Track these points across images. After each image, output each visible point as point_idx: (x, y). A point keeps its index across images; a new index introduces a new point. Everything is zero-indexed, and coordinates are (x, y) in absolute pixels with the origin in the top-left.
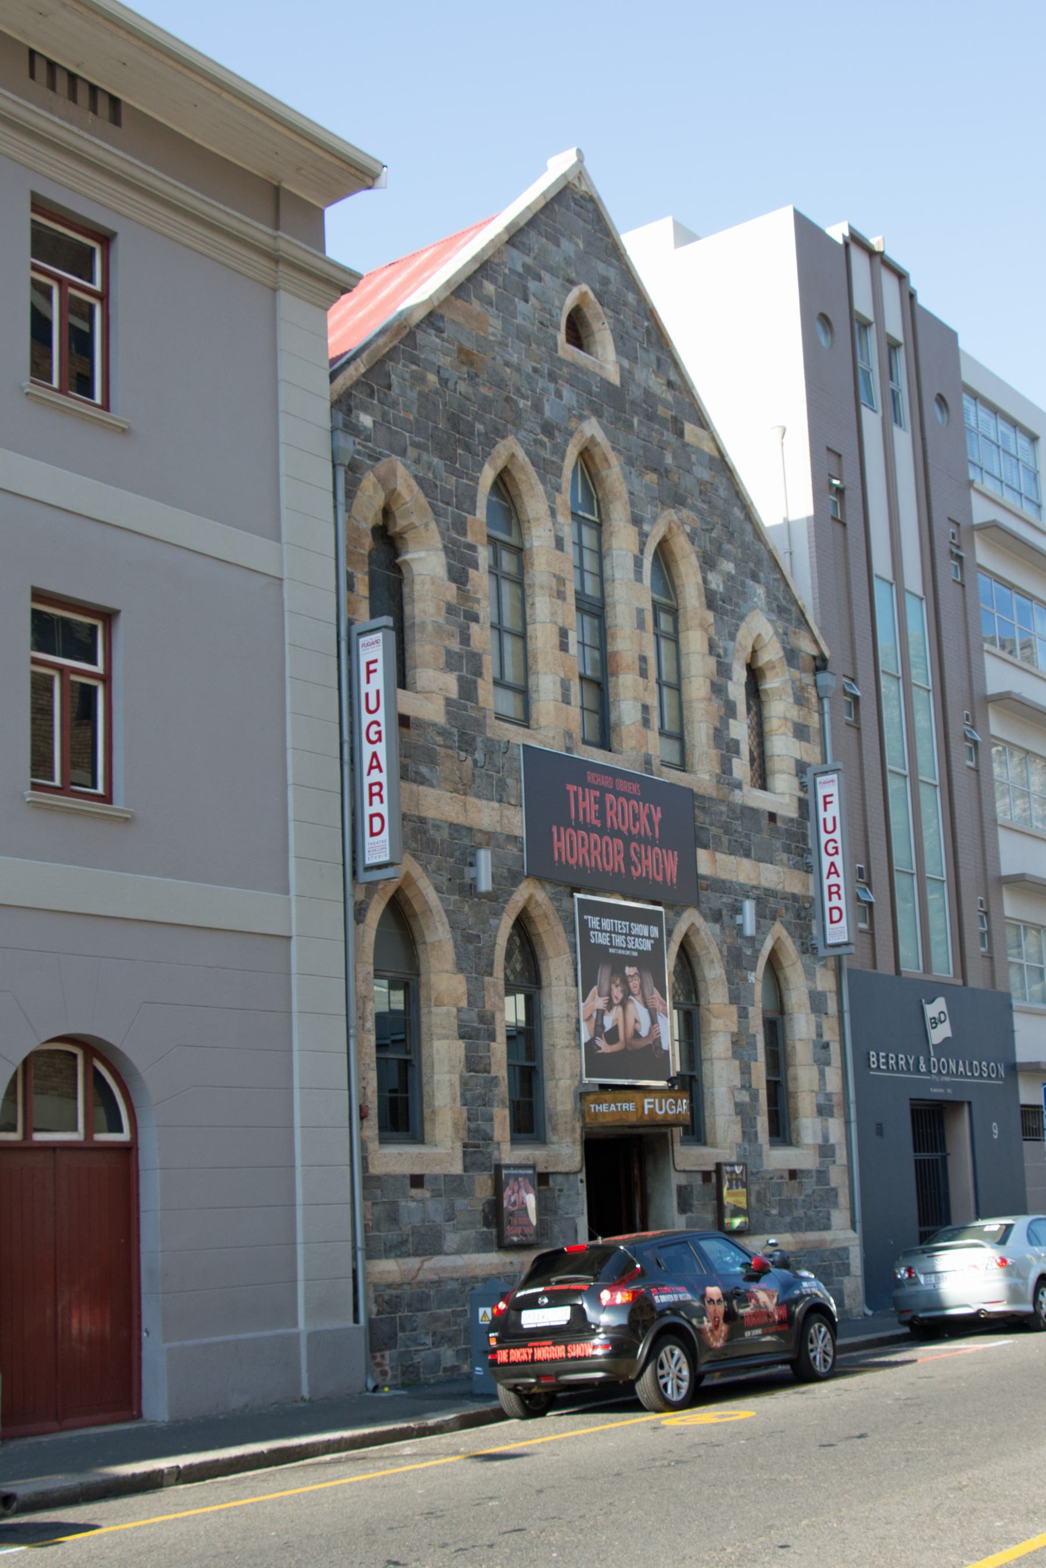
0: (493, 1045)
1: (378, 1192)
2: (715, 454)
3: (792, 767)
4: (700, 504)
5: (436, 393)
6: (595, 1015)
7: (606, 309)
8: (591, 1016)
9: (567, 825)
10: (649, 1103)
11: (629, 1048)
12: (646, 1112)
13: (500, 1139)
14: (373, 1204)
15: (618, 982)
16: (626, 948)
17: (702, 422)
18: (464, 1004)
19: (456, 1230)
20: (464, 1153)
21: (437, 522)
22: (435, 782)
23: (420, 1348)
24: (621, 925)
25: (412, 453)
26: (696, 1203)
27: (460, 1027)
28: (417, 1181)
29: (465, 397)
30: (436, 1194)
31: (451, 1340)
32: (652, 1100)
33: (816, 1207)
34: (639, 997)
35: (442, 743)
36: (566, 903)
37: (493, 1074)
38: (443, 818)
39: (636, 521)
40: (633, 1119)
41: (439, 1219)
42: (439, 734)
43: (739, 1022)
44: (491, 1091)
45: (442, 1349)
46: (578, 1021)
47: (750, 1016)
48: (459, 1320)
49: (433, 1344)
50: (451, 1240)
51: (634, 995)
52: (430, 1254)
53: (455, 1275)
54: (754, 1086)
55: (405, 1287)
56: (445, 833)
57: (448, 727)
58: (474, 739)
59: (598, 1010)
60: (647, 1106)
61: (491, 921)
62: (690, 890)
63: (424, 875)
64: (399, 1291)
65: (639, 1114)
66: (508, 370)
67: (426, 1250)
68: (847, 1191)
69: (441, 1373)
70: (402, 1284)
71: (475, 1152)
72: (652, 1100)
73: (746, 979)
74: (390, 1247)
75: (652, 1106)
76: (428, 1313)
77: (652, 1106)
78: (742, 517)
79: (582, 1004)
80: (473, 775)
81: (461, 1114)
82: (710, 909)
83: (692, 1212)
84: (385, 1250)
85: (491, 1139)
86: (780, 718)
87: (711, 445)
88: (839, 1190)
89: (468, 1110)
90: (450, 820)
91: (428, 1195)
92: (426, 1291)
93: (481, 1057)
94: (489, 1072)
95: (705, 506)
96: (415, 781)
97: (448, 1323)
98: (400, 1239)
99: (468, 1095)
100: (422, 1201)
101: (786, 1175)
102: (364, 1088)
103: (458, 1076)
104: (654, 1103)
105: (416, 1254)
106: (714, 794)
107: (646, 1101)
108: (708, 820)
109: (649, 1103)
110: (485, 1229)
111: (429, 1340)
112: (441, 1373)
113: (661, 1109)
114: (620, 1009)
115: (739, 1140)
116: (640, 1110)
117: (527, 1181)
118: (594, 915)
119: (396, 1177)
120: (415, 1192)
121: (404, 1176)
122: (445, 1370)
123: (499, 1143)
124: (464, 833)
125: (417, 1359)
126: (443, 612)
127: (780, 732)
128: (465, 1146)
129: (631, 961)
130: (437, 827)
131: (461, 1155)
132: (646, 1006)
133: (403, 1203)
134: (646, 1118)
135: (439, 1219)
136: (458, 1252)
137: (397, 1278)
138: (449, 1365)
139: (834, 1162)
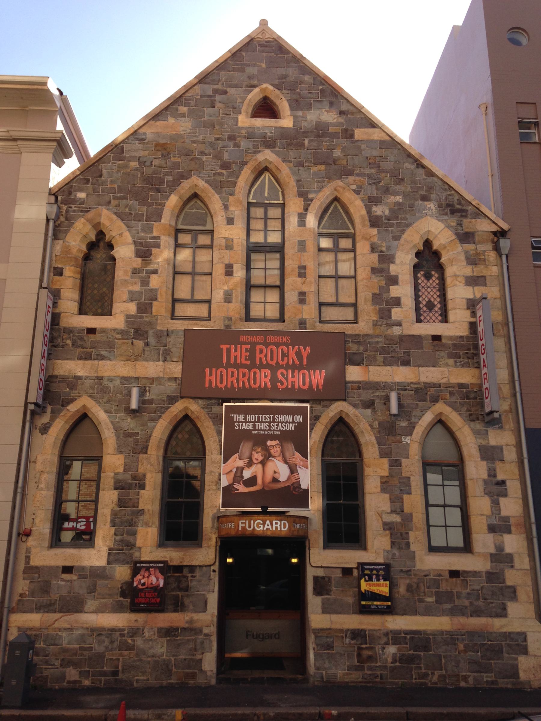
0: (142, 492)
1: (37, 575)
2: (388, 138)
3: (464, 303)
4: (368, 171)
5: (136, 170)
6: (234, 470)
7: (284, 91)
8: (231, 471)
9: (219, 365)
10: (242, 523)
11: (266, 489)
12: (240, 529)
13: (141, 545)
14: (31, 582)
15: (259, 450)
16: (270, 430)
17: (371, 123)
18: (121, 470)
19: (94, 598)
20: (109, 554)
21: (129, 231)
22: (112, 358)
23: (50, 667)
24: (269, 417)
25: (114, 202)
26: (334, 588)
27: (115, 483)
28: (67, 570)
29: (159, 167)
30: (82, 577)
31: (75, 665)
32: (244, 521)
33: (485, 599)
34: (280, 458)
35: (121, 337)
36: (215, 409)
37: (140, 508)
38: (116, 375)
39: (302, 194)
40: (233, 533)
41: (83, 591)
42: (118, 333)
43: (390, 469)
44: (137, 518)
45: (68, 670)
46: (220, 475)
47: (403, 465)
48: (85, 653)
49: (61, 665)
50: (91, 604)
51: (274, 457)
52: (73, 612)
53: (85, 626)
54: (406, 510)
55: (43, 630)
56: (118, 382)
57: (126, 329)
58: (147, 332)
59: (237, 468)
60: (240, 525)
61: (149, 424)
62: (337, 389)
63: (97, 405)
64: (38, 633)
65: (236, 530)
66: (195, 145)
67: (70, 609)
68: (530, 589)
69: (65, 684)
70: (41, 629)
71: (118, 553)
72: (244, 521)
73: (400, 441)
74: (40, 607)
75: (244, 525)
76: (59, 647)
77: (244, 525)
78: (413, 167)
79: (223, 465)
80: (144, 350)
81: (109, 532)
82: (361, 401)
83: (328, 594)
84: (36, 608)
85: (134, 545)
86: (451, 276)
87: (383, 134)
88: (519, 589)
89: (116, 530)
90: (121, 375)
91: (75, 577)
92: (60, 633)
93: (130, 499)
94: (138, 507)
95: (374, 171)
96: (97, 359)
97: (76, 654)
98: (48, 602)
99: (117, 521)
100: (71, 581)
101: (447, 574)
102: (33, 519)
103: (110, 510)
104: (245, 523)
105: (60, 611)
106: (371, 332)
107: (240, 522)
108: (362, 348)
109: (242, 523)
110: (121, 599)
111: (57, 663)
112: (65, 684)
113: (250, 527)
114: (260, 466)
115: (388, 547)
116: (237, 528)
117: (157, 571)
118: (239, 413)
119: (51, 568)
120: (64, 576)
121: (58, 567)
122: (69, 682)
123: (140, 548)
124: (133, 380)
125: (45, 673)
126: (130, 273)
127: (452, 285)
128: (110, 549)
129: (273, 437)
130: (111, 380)
131: (107, 555)
132: (286, 462)
133: (54, 582)
134: (240, 533)
135: (83, 591)
136: (96, 612)
137: (37, 625)
138: (72, 679)
139: (512, 567)
